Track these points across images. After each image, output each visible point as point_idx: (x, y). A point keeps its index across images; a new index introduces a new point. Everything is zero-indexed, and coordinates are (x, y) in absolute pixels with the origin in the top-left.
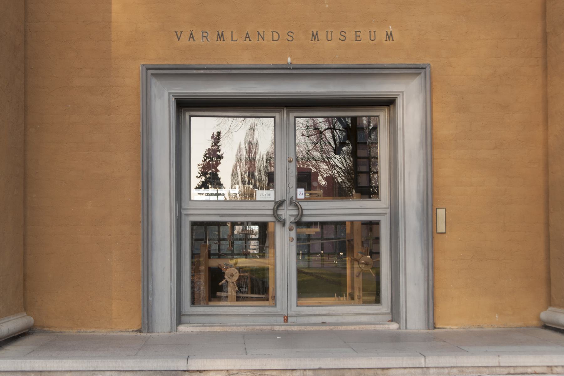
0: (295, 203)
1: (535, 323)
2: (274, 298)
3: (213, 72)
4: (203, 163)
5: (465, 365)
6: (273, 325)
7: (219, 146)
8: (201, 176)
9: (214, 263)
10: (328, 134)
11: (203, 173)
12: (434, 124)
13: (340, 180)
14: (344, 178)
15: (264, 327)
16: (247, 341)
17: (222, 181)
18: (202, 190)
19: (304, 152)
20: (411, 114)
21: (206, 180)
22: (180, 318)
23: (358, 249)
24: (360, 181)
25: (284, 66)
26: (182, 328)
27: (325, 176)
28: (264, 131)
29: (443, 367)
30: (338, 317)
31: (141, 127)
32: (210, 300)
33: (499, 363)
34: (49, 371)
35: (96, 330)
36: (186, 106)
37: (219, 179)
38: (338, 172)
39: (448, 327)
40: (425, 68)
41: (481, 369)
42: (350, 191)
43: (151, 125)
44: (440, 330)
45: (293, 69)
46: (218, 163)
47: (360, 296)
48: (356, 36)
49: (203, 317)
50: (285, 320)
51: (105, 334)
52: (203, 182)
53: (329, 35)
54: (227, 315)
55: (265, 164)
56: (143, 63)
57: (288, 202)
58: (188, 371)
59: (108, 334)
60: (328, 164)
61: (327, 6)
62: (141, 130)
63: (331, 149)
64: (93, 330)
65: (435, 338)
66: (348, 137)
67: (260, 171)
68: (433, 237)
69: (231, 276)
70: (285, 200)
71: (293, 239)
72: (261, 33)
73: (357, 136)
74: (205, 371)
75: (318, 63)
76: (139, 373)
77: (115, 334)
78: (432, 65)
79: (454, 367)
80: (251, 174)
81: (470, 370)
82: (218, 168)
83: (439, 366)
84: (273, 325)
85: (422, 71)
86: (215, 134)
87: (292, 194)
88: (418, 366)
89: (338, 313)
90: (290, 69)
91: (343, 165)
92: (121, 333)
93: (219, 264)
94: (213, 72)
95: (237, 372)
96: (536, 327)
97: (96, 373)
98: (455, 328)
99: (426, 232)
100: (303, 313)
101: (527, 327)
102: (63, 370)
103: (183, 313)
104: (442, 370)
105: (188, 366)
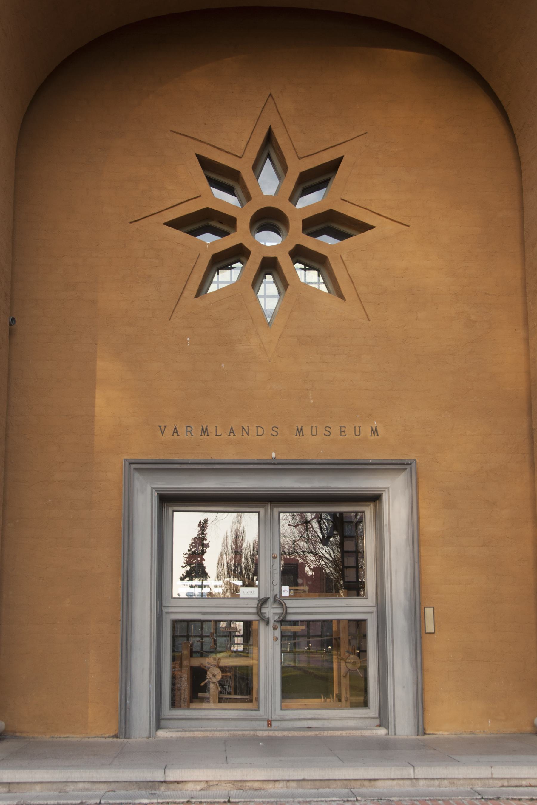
0: (279, 601)
1: (529, 729)
2: (258, 699)
3: (197, 466)
4: (188, 552)
5: (456, 777)
6: (256, 730)
7: (205, 534)
8: (186, 565)
9: (196, 662)
10: (315, 525)
11: (188, 563)
12: (421, 520)
13: (328, 571)
14: (331, 569)
15: (246, 733)
16: (227, 748)
17: (207, 570)
18: (187, 582)
19: (290, 543)
20: (396, 510)
21: (190, 570)
22: (159, 722)
23: (344, 647)
24: (346, 577)
25: (269, 461)
26: (161, 733)
27: (312, 567)
28: (250, 523)
29: (433, 779)
30: (323, 721)
31: (122, 522)
32: (191, 702)
33: (492, 774)
34: (18, 783)
35: (71, 735)
36: (169, 501)
37: (205, 568)
38: (325, 562)
39: (438, 733)
40: (411, 464)
41: (473, 781)
42: (338, 581)
43: (133, 520)
44: (430, 736)
45: (278, 464)
46: (203, 552)
47: (347, 698)
48: (341, 431)
49: (183, 721)
50: (268, 724)
51: (79, 739)
52: (187, 571)
53: (314, 430)
54: (208, 719)
55: (252, 552)
56: (126, 458)
57: (272, 599)
58: (165, 782)
59: (83, 740)
60: (315, 554)
61: (312, 401)
62: (122, 526)
63: (318, 540)
64: (67, 735)
65: (425, 745)
66: (335, 527)
67: (247, 559)
68: (421, 638)
69: (214, 676)
70: (269, 598)
71: (277, 638)
72: (246, 428)
73: (344, 522)
74: (183, 782)
75: (302, 458)
76: (113, 784)
77: (90, 740)
78: (418, 461)
79: (444, 779)
80: (237, 564)
81: (462, 782)
82: (204, 557)
83: (429, 777)
84: (256, 730)
85: (408, 467)
86: (202, 521)
87: (277, 591)
88: (406, 777)
89: (324, 717)
90: (274, 464)
91: (331, 556)
92: (96, 739)
93: (201, 665)
94: (197, 466)
95: (217, 783)
96: (531, 733)
97: (68, 784)
98: (446, 734)
99: (414, 632)
100: (287, 717)
101: (521, 733)
102: (33, 781)
103: (163, 717)
104: (432, 782)
105: (165, 777)
